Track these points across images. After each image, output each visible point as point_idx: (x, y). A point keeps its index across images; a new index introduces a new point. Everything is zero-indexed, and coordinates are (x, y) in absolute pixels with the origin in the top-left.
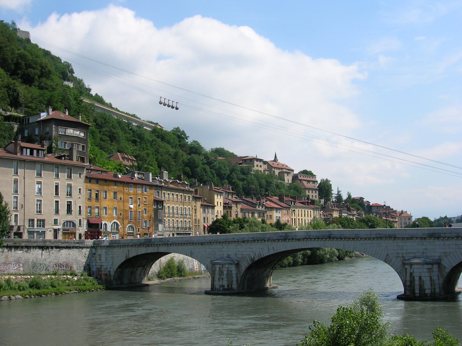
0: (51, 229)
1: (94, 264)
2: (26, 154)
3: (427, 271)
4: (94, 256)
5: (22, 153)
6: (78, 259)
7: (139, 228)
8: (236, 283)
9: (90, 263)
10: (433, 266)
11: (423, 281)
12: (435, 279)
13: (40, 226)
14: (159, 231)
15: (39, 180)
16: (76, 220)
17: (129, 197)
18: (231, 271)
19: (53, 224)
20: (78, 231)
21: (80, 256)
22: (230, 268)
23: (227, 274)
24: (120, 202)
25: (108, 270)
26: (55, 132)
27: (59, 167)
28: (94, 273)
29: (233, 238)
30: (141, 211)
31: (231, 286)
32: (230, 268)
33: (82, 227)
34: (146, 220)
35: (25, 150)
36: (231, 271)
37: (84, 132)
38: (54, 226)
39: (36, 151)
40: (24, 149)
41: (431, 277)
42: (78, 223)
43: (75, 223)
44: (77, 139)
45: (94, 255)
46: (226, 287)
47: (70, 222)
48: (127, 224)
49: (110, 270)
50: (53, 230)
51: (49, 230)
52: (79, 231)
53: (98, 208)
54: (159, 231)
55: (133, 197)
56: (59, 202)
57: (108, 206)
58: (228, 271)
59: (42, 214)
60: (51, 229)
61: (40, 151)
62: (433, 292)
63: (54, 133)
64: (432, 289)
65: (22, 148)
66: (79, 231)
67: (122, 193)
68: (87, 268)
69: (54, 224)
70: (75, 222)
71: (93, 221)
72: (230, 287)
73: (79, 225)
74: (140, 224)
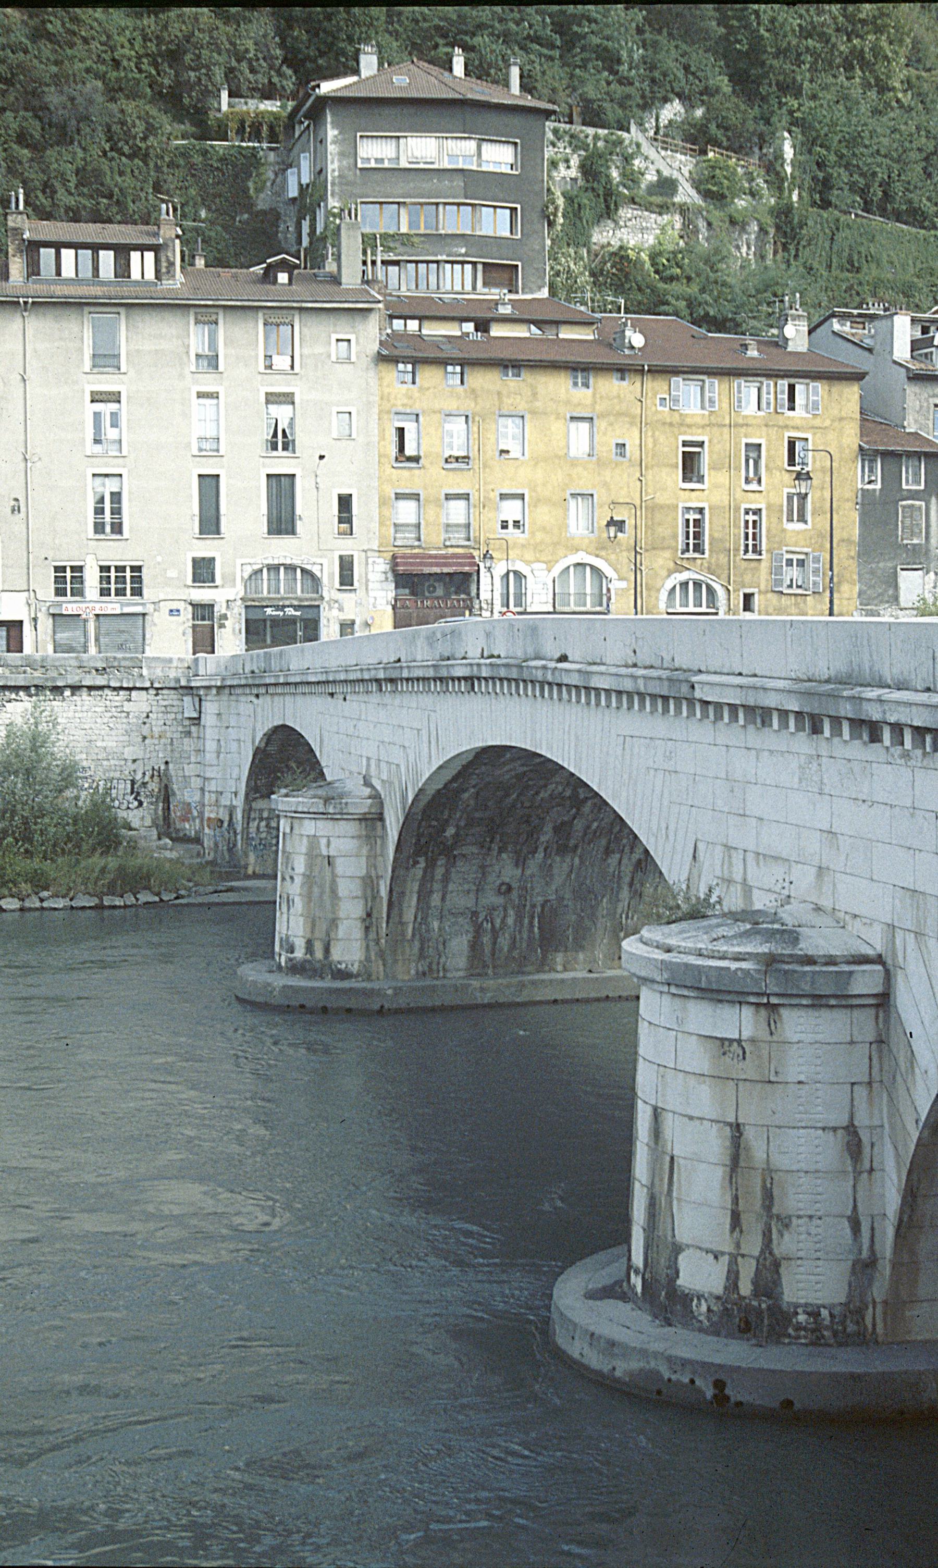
0: (181, 606)
1: (190, 770)
2: (58, 273)
3: (705, 1068)
4: (195, 735)
5: (33, 269)
6: (99, 744)
7: (755, 590)
8: (357, 933)
9: (171, 766)
10: (772, 1025)
11: (672, 1158)
12: (780, 1161)
13: (120, 592)
14: (903, 605)
15: (106, 384)
16: (319, 561)
17: (682, 438)
18: (330, 860)
19: (190, 582)
20: (335, 612)
21: (113, 732)
22: (323, 841)
23: (309, 879)
24: (622, 463)
25: (225, 801)
26: (339, 161)
27: (221, 321)
28: (190, 812)
29: (563, 658)
30: (769, 507)
31: (327, 950)
32: (323, 841)
33: (361, 593)
34: (806, 554)
35: (47, 254)
36: (330, 860)
37: (516, 144)
38: (192, 590)
39: (112, 253)
40: (132, 253)
41: (737, 1128)
42: (331, 575)
43: (318, 574)
44: (459, 183)
45: (193, 729)
46: (299, 954)
47: (291, 568)
48: (664, 573)
49: (234, 803)
50: (190, 608)
51: (165, 607)
52: (341, 609)
53: (468, 499)
54: (903, 605)
55: (705, 438)
56: (222, 480)
57: (533, 489)
58: (312, 855)
59: (125, 537)
60: (181, 606)
61: (135, 256)
62: (746, 1288)
63: (336, 165)
64: (734, 1260)
65: (33, 247)
66: (341, 609)
67: (632, 424)
68: (154, 786)
69: (194, 581)
70: (316, 570)
71: (421, 564)
72: (319, 955)
73: (337, 585)
74: (757, 569)
